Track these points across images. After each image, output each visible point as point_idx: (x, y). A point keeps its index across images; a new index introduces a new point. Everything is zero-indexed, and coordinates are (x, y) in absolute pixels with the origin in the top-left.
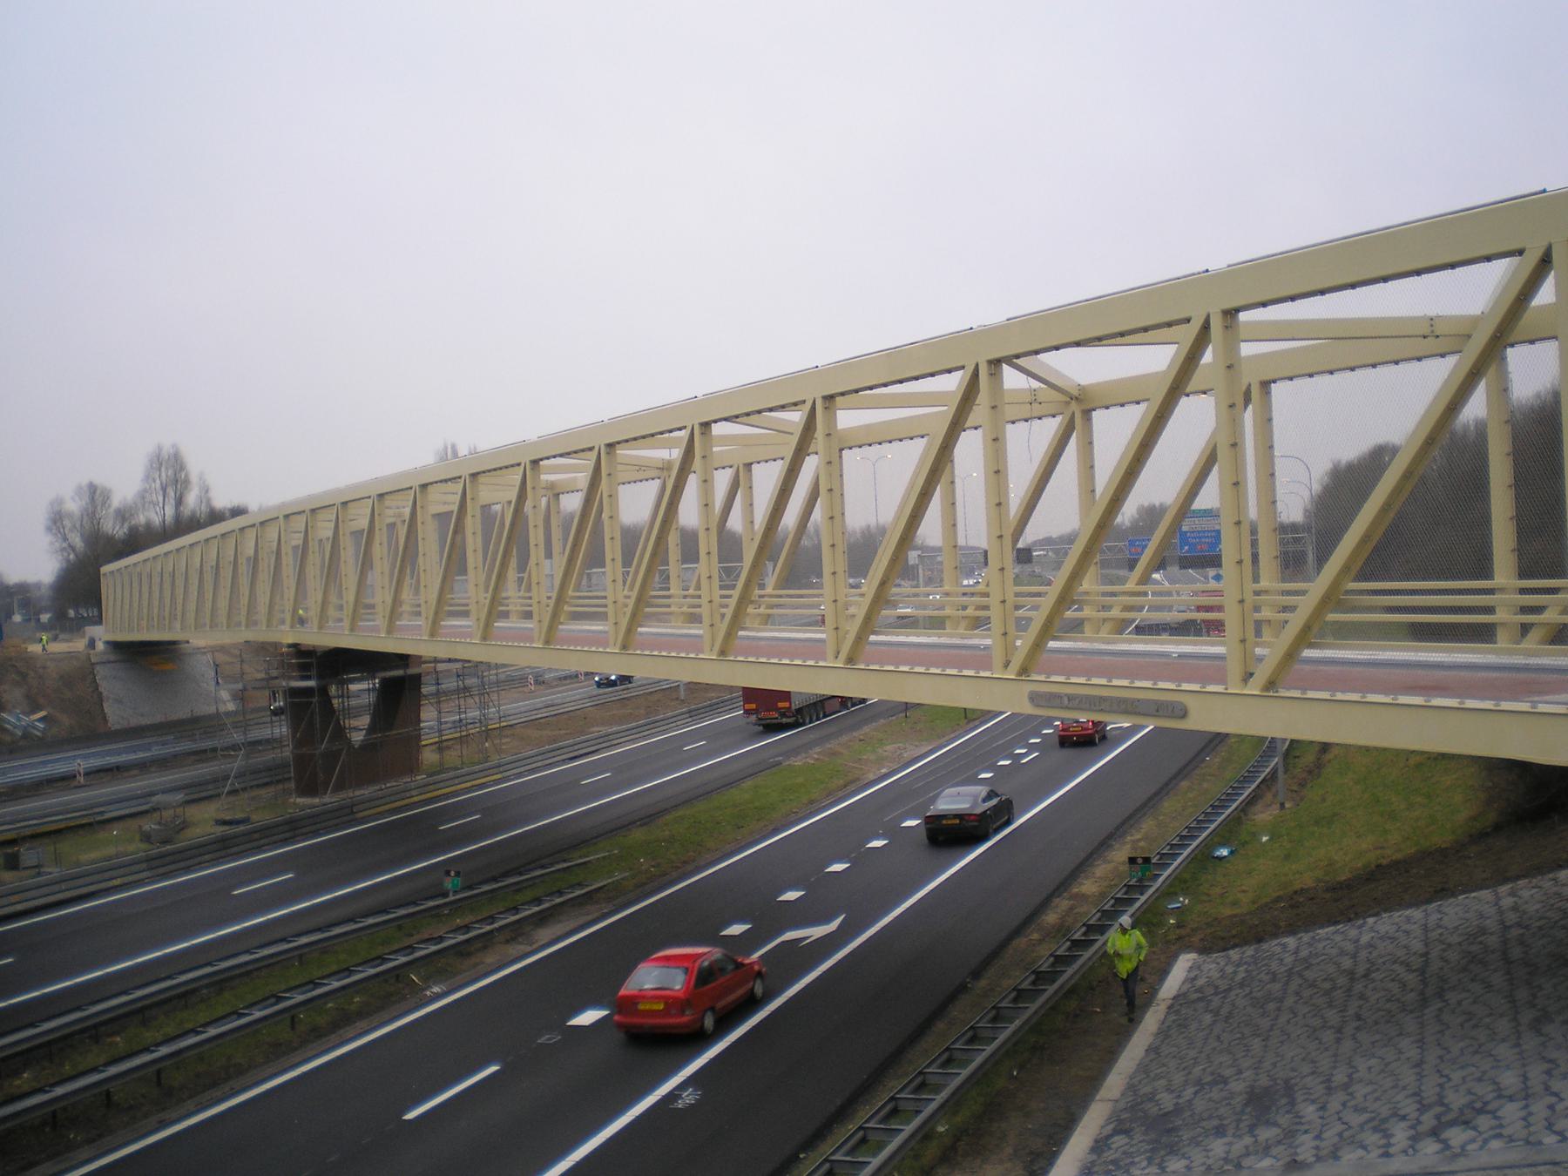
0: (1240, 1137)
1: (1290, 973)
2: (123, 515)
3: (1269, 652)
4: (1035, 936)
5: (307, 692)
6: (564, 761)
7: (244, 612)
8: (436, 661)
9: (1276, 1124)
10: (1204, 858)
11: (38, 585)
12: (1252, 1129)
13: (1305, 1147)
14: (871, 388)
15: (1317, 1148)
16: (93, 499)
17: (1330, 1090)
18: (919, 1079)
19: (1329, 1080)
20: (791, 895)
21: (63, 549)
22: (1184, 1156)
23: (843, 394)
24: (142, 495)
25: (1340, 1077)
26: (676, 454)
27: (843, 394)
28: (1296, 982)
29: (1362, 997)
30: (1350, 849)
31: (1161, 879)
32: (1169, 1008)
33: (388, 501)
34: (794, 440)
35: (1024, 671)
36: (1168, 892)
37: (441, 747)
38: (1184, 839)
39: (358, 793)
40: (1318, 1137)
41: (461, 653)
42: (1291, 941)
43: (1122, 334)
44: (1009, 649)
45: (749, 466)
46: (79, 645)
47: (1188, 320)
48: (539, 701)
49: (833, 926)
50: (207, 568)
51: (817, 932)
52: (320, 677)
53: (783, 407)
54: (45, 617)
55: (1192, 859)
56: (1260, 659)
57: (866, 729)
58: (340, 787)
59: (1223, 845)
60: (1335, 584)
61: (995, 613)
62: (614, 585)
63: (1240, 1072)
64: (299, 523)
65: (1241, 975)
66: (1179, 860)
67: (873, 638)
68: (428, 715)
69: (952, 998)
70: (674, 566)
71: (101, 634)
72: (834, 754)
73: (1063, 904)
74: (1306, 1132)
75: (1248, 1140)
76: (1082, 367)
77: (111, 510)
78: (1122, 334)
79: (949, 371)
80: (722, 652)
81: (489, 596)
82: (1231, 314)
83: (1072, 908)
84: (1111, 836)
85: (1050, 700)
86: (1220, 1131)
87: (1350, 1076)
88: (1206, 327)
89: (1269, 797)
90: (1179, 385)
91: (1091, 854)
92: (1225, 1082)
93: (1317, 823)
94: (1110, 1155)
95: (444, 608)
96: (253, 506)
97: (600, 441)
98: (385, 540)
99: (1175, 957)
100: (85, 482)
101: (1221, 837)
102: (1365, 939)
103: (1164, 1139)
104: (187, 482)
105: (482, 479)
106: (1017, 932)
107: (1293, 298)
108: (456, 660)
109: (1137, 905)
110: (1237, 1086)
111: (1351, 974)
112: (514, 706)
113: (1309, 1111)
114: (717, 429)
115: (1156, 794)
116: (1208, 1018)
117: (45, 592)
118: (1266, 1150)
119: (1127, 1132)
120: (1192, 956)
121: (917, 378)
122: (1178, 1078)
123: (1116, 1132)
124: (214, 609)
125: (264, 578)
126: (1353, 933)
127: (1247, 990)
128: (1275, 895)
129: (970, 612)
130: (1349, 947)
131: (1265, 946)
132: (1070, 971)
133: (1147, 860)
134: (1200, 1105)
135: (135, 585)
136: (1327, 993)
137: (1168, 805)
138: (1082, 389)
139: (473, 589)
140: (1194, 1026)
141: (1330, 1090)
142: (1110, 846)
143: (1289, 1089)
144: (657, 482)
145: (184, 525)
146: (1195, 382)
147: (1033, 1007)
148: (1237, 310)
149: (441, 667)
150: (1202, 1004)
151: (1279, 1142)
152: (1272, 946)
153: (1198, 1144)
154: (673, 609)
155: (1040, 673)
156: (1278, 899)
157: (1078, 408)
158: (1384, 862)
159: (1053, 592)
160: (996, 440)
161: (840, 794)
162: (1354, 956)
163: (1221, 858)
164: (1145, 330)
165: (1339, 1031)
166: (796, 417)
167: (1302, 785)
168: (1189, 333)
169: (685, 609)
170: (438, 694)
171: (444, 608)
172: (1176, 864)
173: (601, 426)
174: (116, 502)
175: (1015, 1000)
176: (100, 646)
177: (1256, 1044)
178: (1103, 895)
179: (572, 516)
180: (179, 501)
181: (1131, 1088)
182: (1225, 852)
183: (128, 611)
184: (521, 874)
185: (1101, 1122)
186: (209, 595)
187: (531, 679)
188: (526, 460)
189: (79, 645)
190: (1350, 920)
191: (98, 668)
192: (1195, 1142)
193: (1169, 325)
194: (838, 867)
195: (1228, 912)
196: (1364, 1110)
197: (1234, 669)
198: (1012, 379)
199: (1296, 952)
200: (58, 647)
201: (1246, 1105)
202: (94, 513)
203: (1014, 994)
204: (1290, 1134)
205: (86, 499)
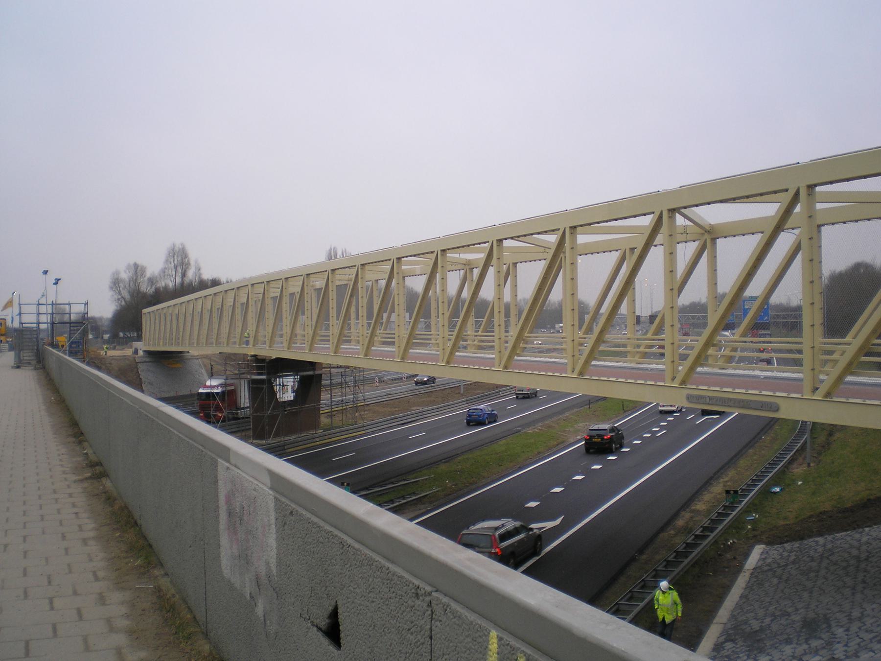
0: (800, 645)
1: (822, 556)
2: (151, 281)
3: (827, 379)
4: (672, 532)
5: (261, 382)
6: (398, 425)
7: (215, 337)
8: (330, 367)
9: (820, 638)
10: (766, 493)
11: (101, 319)
12: (807, 641)
13: (839, 651)
14: (598, 223)
15: (846, 651)
16: (136, 272)
17: (851, 620)
18: (616, 607)
19: (850, 615)
20: (533, 504)
21: (119, 299)
22: (768, 654)
23: (581, 226)
24: (164, 271)
25: (856, 614)
26: (482, 256)
27: (581, 226)
28: (825, 563)
29: (865, 571)
30: (851, 490)
31: (743, 503)
32: (752, 574)
33: (312, 278)
34: (552, 252)
35: (683, 382)
36: (747, 511)
37: (331, 415)
38: (755, 482)
39: (286, 438)
40: (846, 645)
41: (352, 363)
42: (821, 540)
43: (747, 197)
44: (675, 371)
45: (515, 264)
46: (129, 352)
47: (787, 190)
48: (382, 392)
49: (558, 521)
50: (215, 310)
51: (549, 525)
52: (268, 374)
53: (546, 232)
54: (106, 336)
55: (759, 493)
56: (822, 381)
57: (567, 414)
58: (277, 435)
59: (776, 486)
60: (868, 340)
61: (667, 351)
62: (440, 329)
63: (797, 610)
64: (260, 289)
65: (792, 558)
66: (753, 493)
67: (594, 363)
68: (325, 397)
69: (627, 564)
70: (353, 321)
71: (141, 346)
72: (550, 427)
73: (686, 515)
74: (839, 643)
75: (805, 646)
76: (713, 215)
77: (146, 278)
78: (747, 197)
79: (645, 215)
80: (506, 367)
81: (370, 332)
82: (811, 187)
83: (692, 518)
84: (711, 478)
85: (699, 399)
86: (788, 641)
87: (862, 613)
88: (797, 194)
89: (800, 459)
90: (779, 227)
91: (701, 488)
92: (789, 615)
93: (830, 475)
94: (724, 653)
95: (343, 338)
96: (223, 279)
97: (438, 248)
98: (288, 301)
99: (752, 547)
100: (132, 263)
101: (776, 481)
102: (864, 539)
103: (755, 645)
104: (188, 264)
105: (367, 267)
106: (662, 529)
107: (848, 180)
108: (341, 367)
109: (731, 517)
110: (797, 618)
111: (858, 558)
112: (371, 394)
113: (840, 632)
114: (506, 243)
115: (735, 456)
116: (775, 581)
117: (106, 323)
118: (816, 652)
119: (733, 641)
120: (763, 546)
121: (625, 218)
122: (761, 613)
123: (726, 641)
124: (218, 334)
125: (226, 319)
126: (857, 536)
127: (797, 565)
128: (809, 514)
129: (642, 349)
130: (855, 543)
131: (805, 542)
132: (696, 552)
133: (736, 492)
134: (775, 627)
135: (157, 321)
136: (845, 568)
137: (742, 462)
138: (711, 226)
139: (359, 328)
140: (767, 585)
141: (851, 620)
142: (711, 484)
143: (827, 620)
144: (462, 272)
145: (184, 290)
146: (790, 223)
147: (677, 570)
148: (816, 185)
149: (333, 371)
150: (770, 573)
151: (824, 648)
152: (810, 542)
153: (776, 648)
154: (433, 341)
155: (692, 384)
156: (811, 517)
157: (709, 237)
158: (872, 497)
159: (702, 339)
160: (671, 253)
161: (555, 449)
162: (859, 549)
163: (775, 493)
164: (761, 195)
165: (854, 589)
166: (553, 239)
167: (819, 454)
168: (787, 197)
169: (476, 343)
170: (331, 385)
171: (343, 338)
172: (751, 495)
173: (438, 240)
174: (148, 274)
175: (665, 566)
176: (141, 353)
177: (805, 595)
178: (709, 511)
179: (724, 296)
180: (184, 275)
181: (733, 616)
182: (777, 489)
183: (156, 334)
184: (381, 486)
185: (718, 635)
186: (216, 326)
187: (377, 379)
188: (394, 257)
189: (129, 352)
190: (855, 529)
191: (139, 365)
192: (774, 647)
193: (775, 192)
194: (557, 490)
195: (782, 523)
196: (872, 631)
197: (807, 386)
198: (680, 220)
199: (824, 545)
200: (111, 353)
201: (802, 628)
202: (136, 280)
203: (665, 563)
204: (829, 644)
205: (132, 271)
